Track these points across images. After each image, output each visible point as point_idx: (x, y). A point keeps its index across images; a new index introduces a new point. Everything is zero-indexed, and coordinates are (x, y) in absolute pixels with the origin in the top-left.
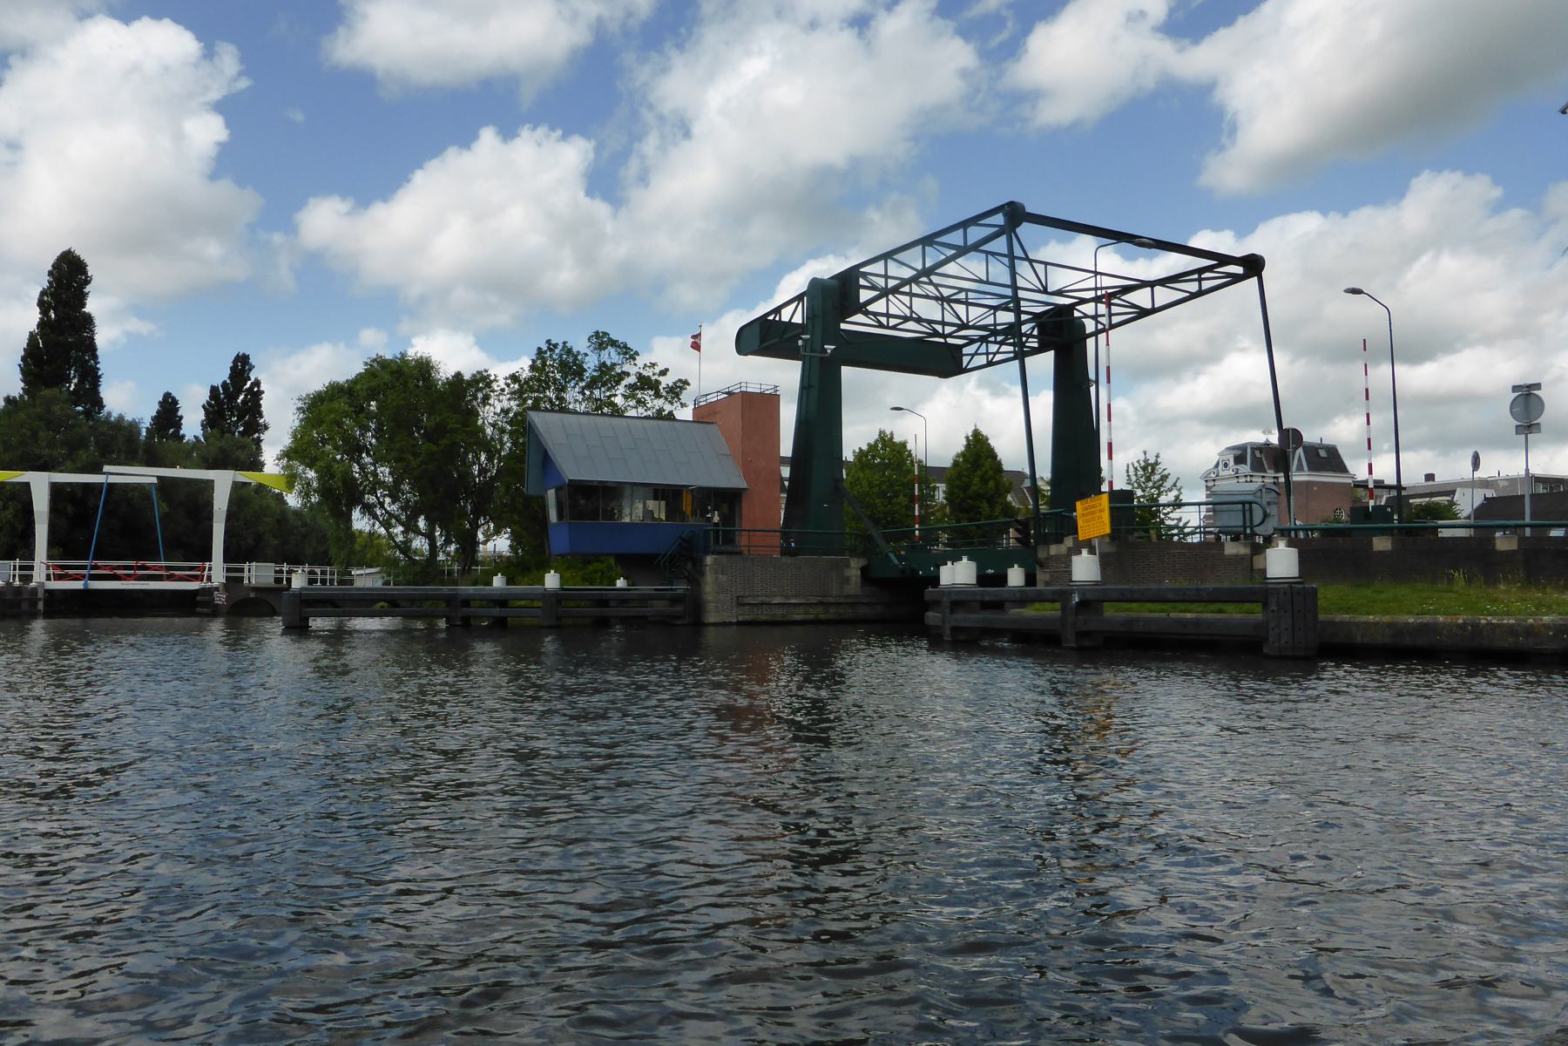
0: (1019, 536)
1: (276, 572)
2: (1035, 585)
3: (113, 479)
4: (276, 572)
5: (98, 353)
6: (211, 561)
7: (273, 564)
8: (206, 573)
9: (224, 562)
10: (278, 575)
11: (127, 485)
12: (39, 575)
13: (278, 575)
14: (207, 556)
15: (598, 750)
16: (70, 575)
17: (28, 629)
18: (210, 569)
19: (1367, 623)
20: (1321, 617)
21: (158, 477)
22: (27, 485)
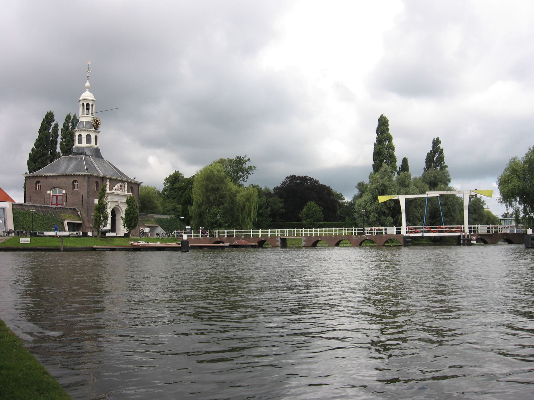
0: (435, 139)
1: (488, 228)
2: (82, 143)
3: (429, 196)
4: (488, 228)
5: (389, 127)
6: (464, 225)
7: (486, 225)
8: (462, 229)
9: (469, 225)
10: (489, 229)
11: (432, 197)
12: (404, 232)
13: (489, 229)
14: (463, 223)
15: (437, 309)
16: (452, 231)
17: (30, 295)
18: (464, 228)
19: (160, 392)
20: (20, 242)
21: (440, 194)
22: (86, 143)
